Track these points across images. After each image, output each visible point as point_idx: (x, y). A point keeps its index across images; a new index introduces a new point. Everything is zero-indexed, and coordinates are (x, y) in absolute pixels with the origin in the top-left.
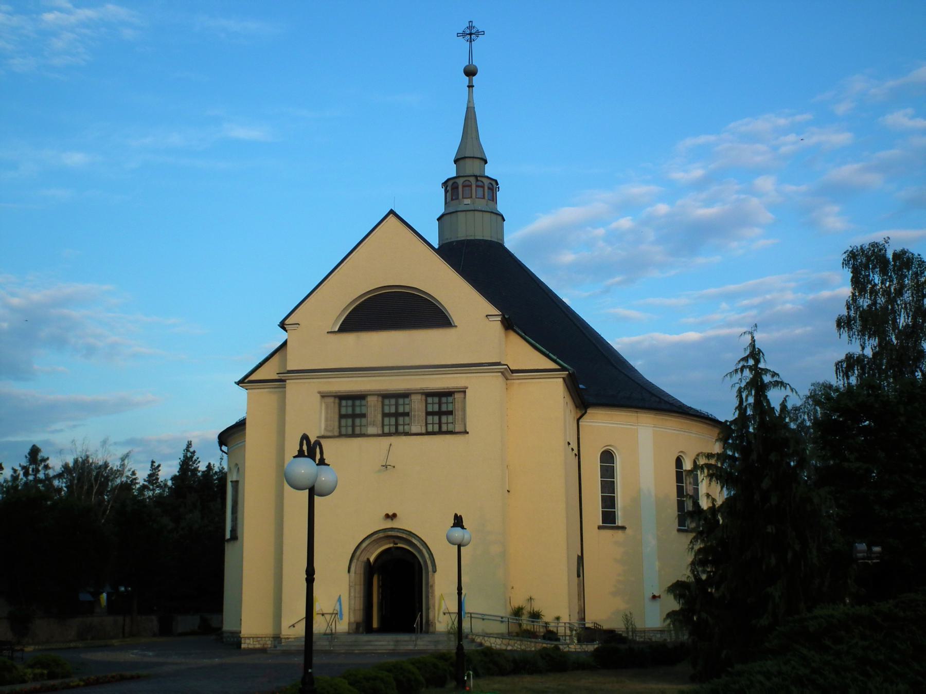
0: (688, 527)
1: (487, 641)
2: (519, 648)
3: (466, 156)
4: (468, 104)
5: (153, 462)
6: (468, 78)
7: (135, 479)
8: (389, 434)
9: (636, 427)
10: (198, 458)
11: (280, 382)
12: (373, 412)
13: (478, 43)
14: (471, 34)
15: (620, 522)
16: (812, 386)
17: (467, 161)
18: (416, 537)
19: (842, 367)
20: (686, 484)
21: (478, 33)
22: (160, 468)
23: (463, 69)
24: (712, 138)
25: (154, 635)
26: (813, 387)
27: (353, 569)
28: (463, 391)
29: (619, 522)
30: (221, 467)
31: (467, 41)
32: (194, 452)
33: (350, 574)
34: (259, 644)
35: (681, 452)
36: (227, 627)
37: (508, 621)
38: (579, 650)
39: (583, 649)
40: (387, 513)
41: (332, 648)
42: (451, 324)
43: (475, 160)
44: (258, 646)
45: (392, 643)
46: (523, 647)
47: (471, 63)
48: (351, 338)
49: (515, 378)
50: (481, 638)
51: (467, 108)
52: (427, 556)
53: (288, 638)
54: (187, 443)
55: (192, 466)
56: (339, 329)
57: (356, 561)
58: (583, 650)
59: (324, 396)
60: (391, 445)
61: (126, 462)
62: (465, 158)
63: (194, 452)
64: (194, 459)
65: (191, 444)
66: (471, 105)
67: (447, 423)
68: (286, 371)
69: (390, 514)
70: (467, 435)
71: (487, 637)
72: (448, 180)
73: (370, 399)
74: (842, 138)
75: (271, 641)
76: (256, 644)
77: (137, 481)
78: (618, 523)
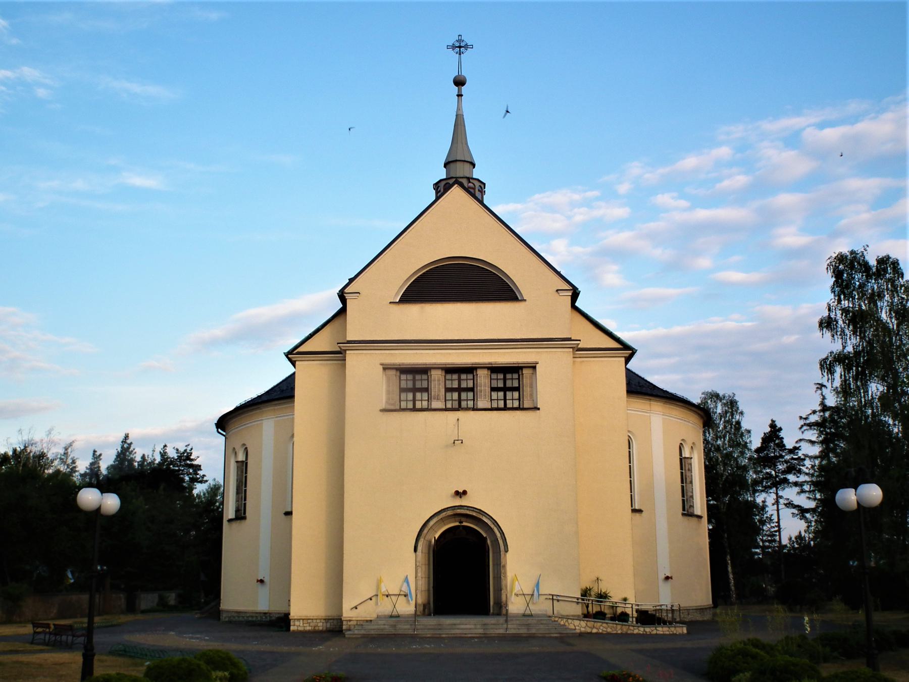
0: (688, 511)
1: (571, 623)
2: (604, 631)
3: (458, 159)
4: (457, 112)
5: (95, 451)
6: (457, 88)
7: (75, 467)
8: (452, 409)
9: (649, 415)
10: (134, 449)
11: (338, 355)
13: (467, 55)
14: (460, 47)
15: (636, 505)
16: (702, 394)
17: (458, 164)
18: (486, 515)
19: (826, 364)
20: (685, 470)
21: (466, 47)
22: (101, 457)
23: (454, 77)
24: (519, 206)
25: (122, 613)
26: (703, 396)
27: (420, 548)
30: (153, 458)
31: (457, 53)
32: (131, 443)
33: (417, 553)
34: (310, 626)
35: (683, 440)
37: (592, 603)
38: (668, 633)
39: (672, 631)
40: (457, 490)
41: (416, 632)
43: (465, 163)
44: (308, 628)
45: (478, 626)
46: (609, 630)
47: (460, 74)
48: (414, 310)
49: (578, 356)
50: (565, 620)
51: (457, 115)
52: (498, 535)
53: (350, 621)
54: (124, 435)
55: (129, 456)
56: (399, 300)
57: (423, 540)
58: (671, 633)
59: (386, 368)
60: (458, 419)
61: (69, 450)
62: (456, 161)
63: (131, 443)
64: (130, 450)
65: (128, 437)
66: (460, 113)
67: (498, 400)
68: (346, 342)
69: (461, 491)
70: (538, 411)
71: (571, 619)
72: (441, 181)
73: (433, 372)
74: (620, 212)
75: (323, 623)
76: (306, 626)
77: (76, 469)
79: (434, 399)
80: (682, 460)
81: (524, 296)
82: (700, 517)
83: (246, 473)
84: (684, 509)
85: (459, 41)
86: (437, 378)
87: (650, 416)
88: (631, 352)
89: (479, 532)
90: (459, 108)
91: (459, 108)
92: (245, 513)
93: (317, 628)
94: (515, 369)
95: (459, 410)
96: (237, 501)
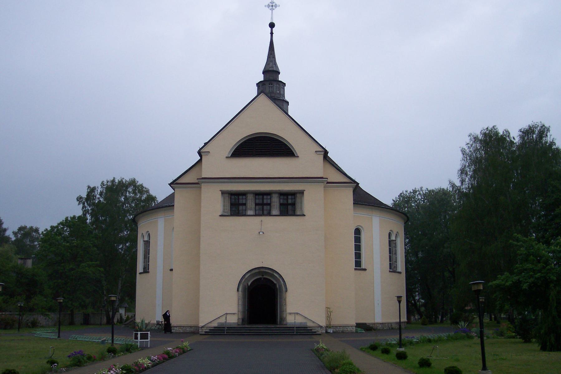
12: (250, 203)
20: (392, 247)
27: (240, 289)
28: (302, 192)
29: (363, 266)
35: (391, 230)
42: (295, 156)
59: (223, 193)
60: (262, 221)
68: (201, 178)
73: (248, 195)
78: (362, 267)
79: (249, 209)
80: (390, 242)
81: (298, 153)
82: (400, 273)
83: (149, 247)
84: (390, 268)
86: (250, 198)
87: (372, 217)
88: (356, 184)
89: (272, 281)
92: (148, 270)
93: (186, 331)
94: (294, 194)
95: (262, 216)
96: (144, 262)
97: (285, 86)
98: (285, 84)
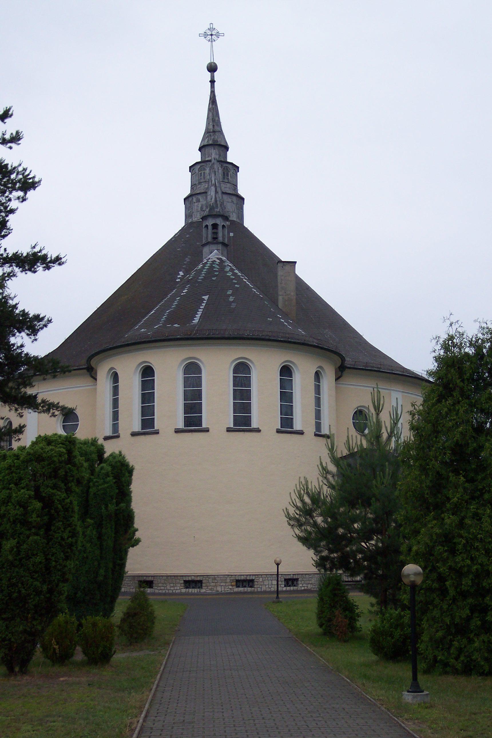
6: (210, 73)
13: (218, 43)
36: (32, 380)
69: (35, 342)
72: (197, 163)
85: (211, 29)
90: (213, 92)
91: (213, 92)
97: (238, 172)
98: (238, 168)
